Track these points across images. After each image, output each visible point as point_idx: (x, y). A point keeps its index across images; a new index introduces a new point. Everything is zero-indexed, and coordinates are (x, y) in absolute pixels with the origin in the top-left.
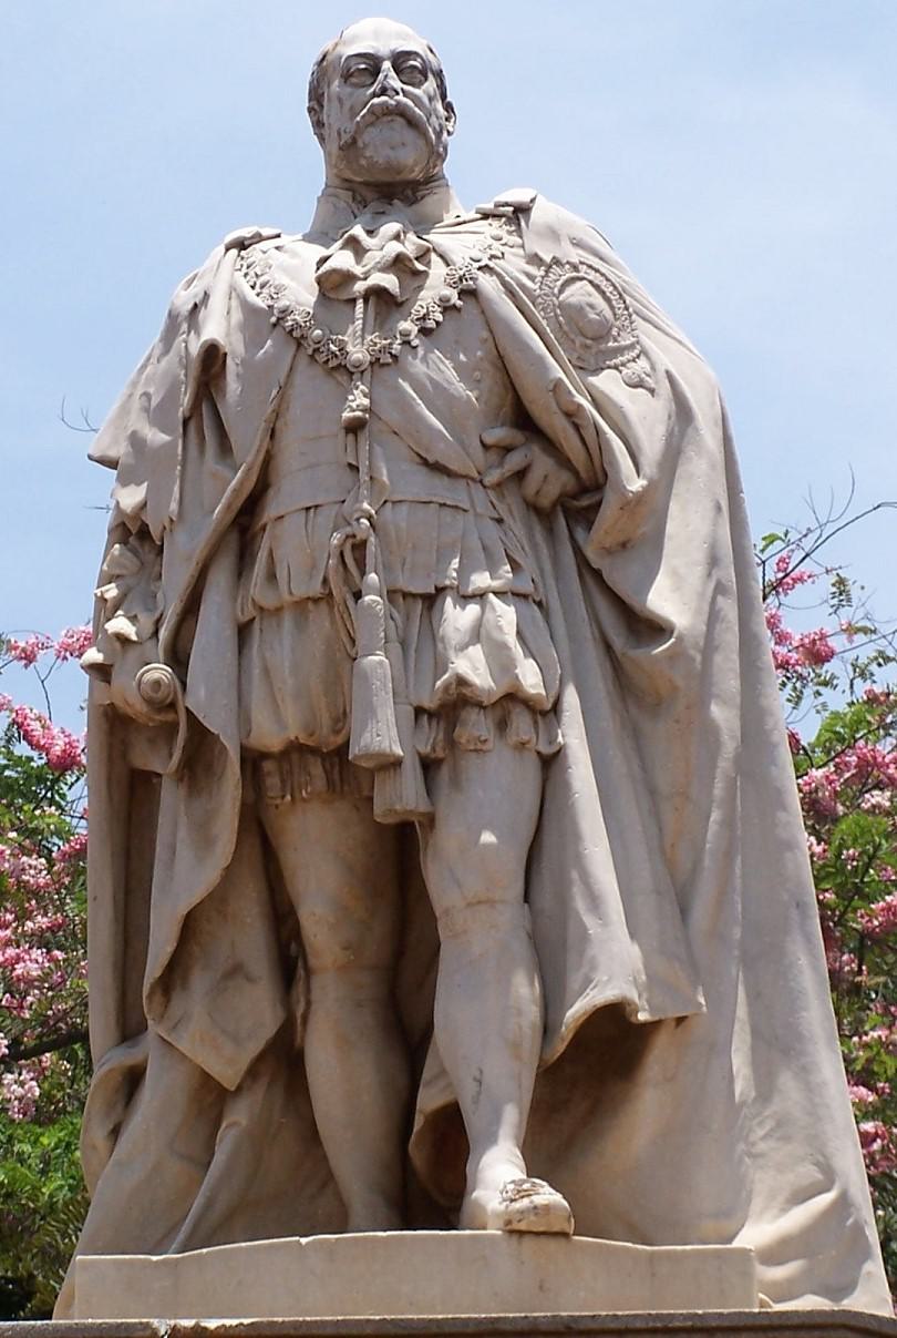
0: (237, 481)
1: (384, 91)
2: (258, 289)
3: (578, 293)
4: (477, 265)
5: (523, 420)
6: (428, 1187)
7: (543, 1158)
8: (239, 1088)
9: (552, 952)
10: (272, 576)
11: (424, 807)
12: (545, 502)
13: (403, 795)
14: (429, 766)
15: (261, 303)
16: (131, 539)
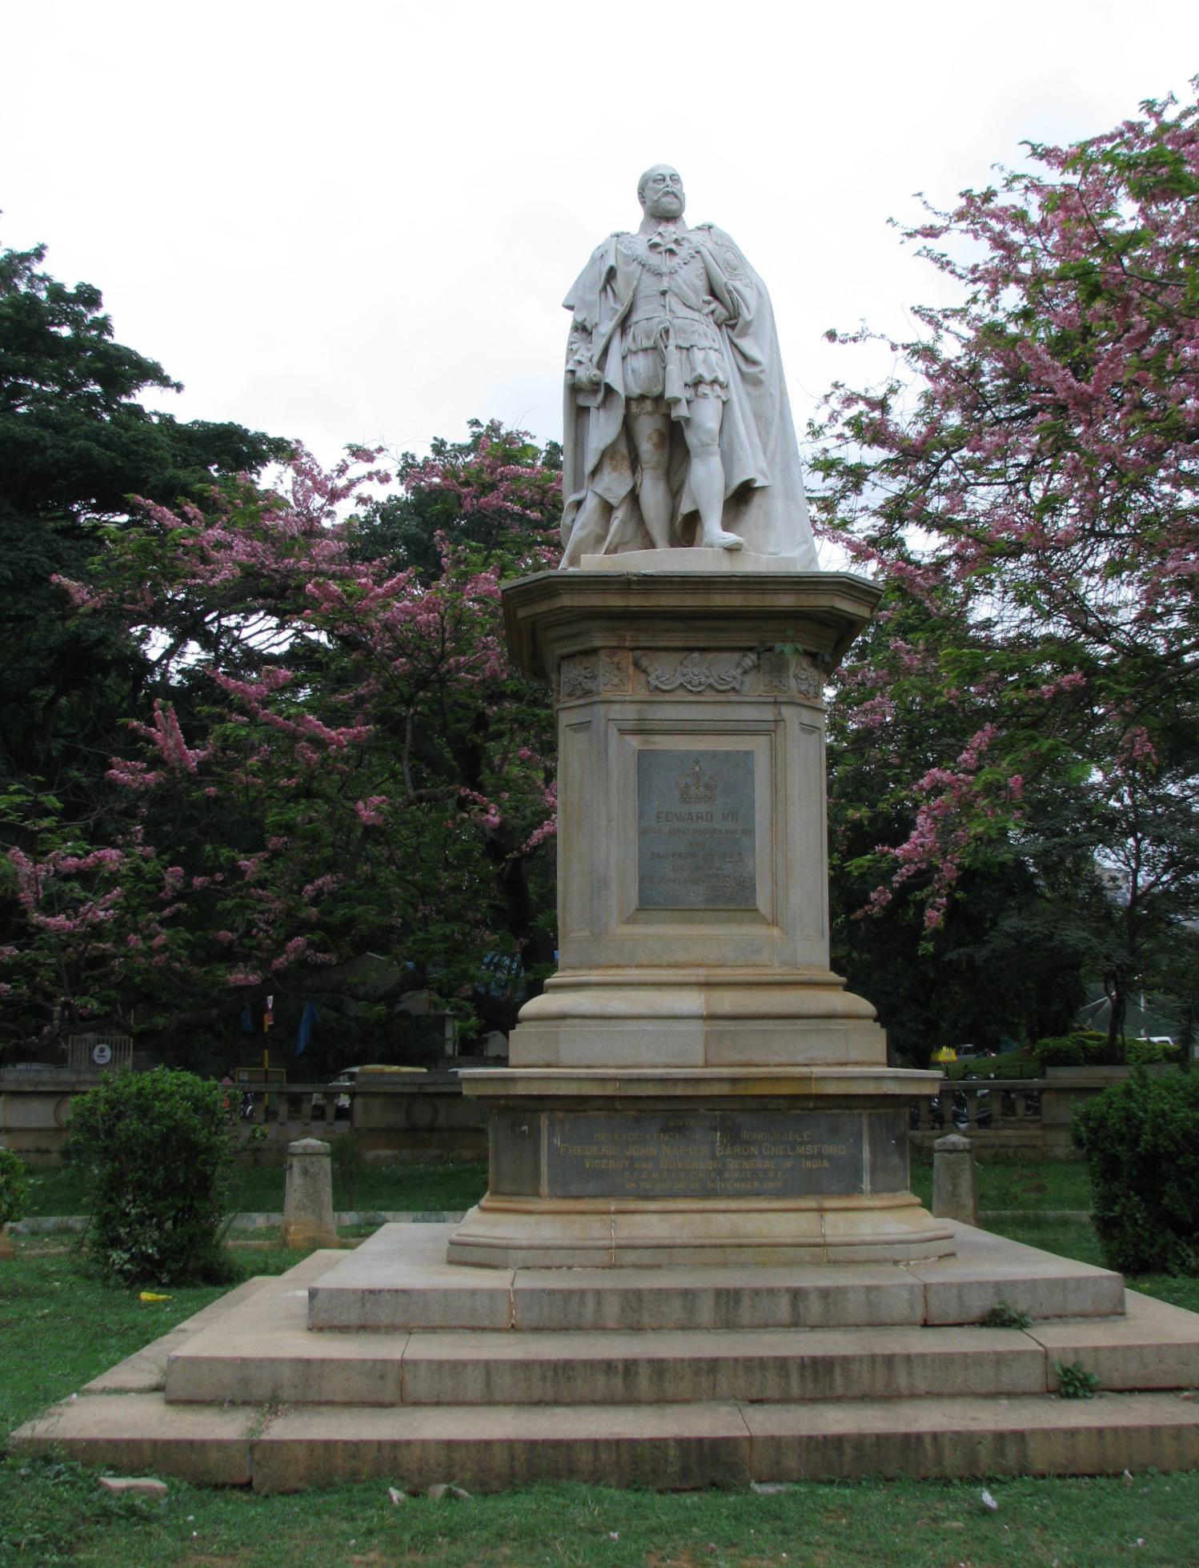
0: (621, 309)
3: (729, 256)
6: (687, 530)
9: (728, 461)
13: (682, 411)
14: (689, 402)
15: (629, 253)
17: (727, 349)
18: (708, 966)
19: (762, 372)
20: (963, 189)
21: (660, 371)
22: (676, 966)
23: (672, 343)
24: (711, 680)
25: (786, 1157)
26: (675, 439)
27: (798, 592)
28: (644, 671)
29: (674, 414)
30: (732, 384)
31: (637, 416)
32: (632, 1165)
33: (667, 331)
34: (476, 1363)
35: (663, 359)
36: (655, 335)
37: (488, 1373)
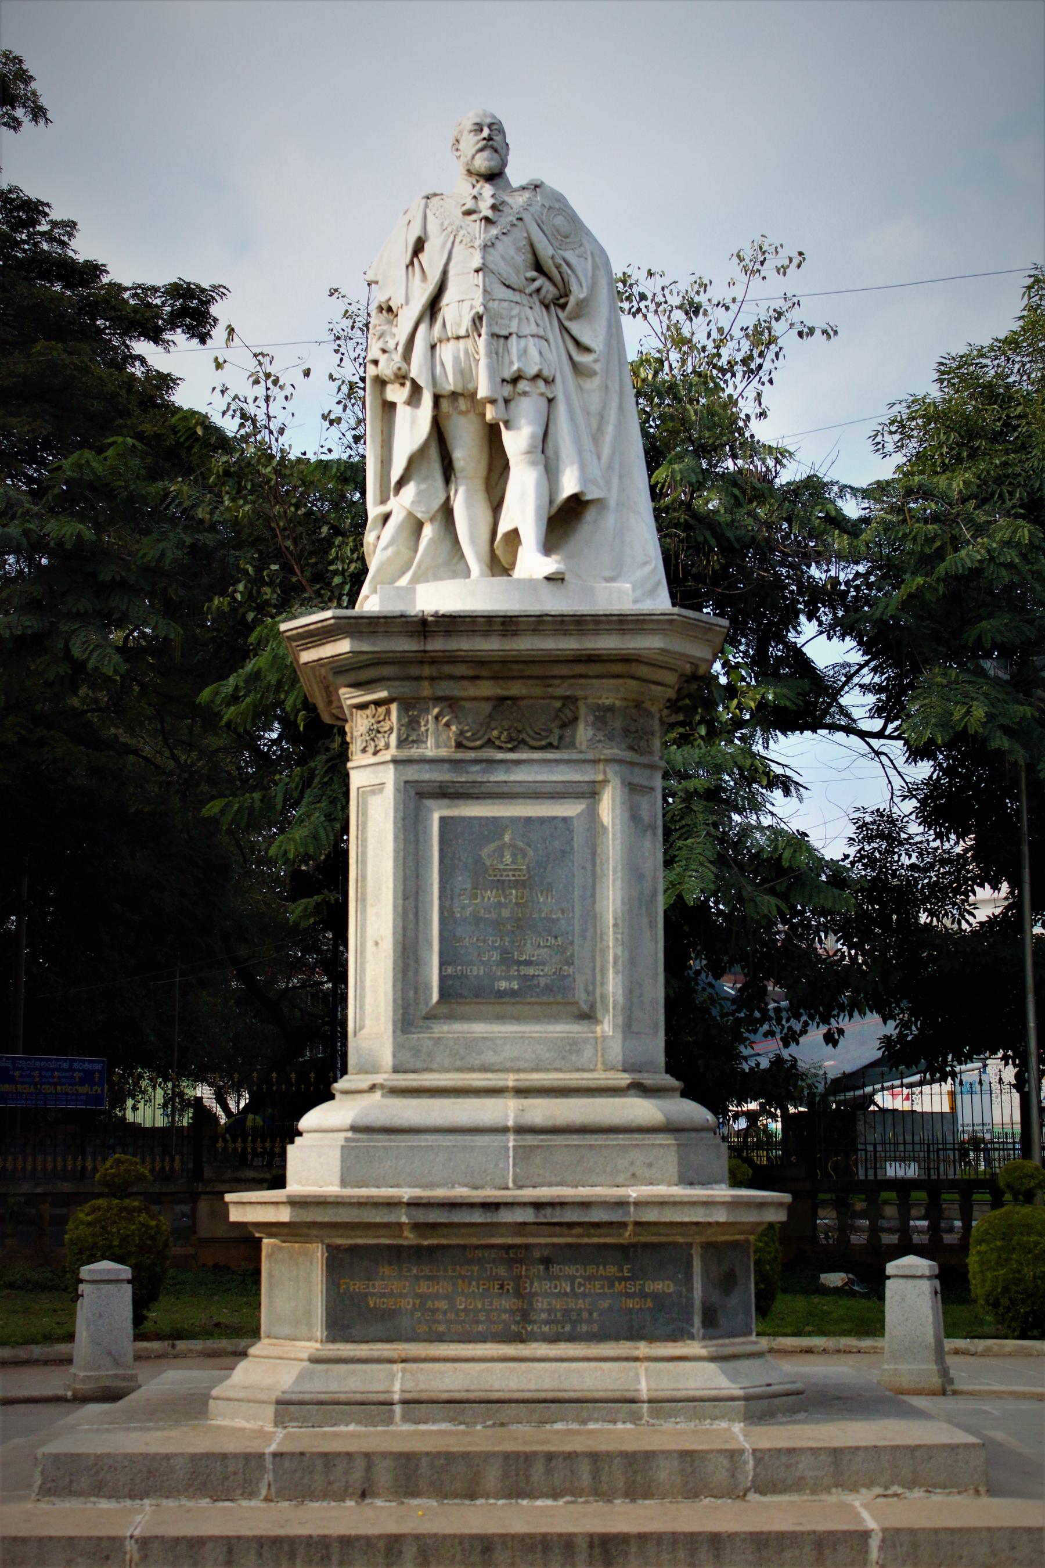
5: (538, 267)
7: (548, 547)
14: (507, 401)
17: (554, 333)
18: (519, 1071)
20: (227, 385)
22: (484, 1069)
25: (604, 1295)
27: (623, 631)
31: (448, 416)
32: (423, 1304)
34: (215, 1539)
37: (230, 1551)
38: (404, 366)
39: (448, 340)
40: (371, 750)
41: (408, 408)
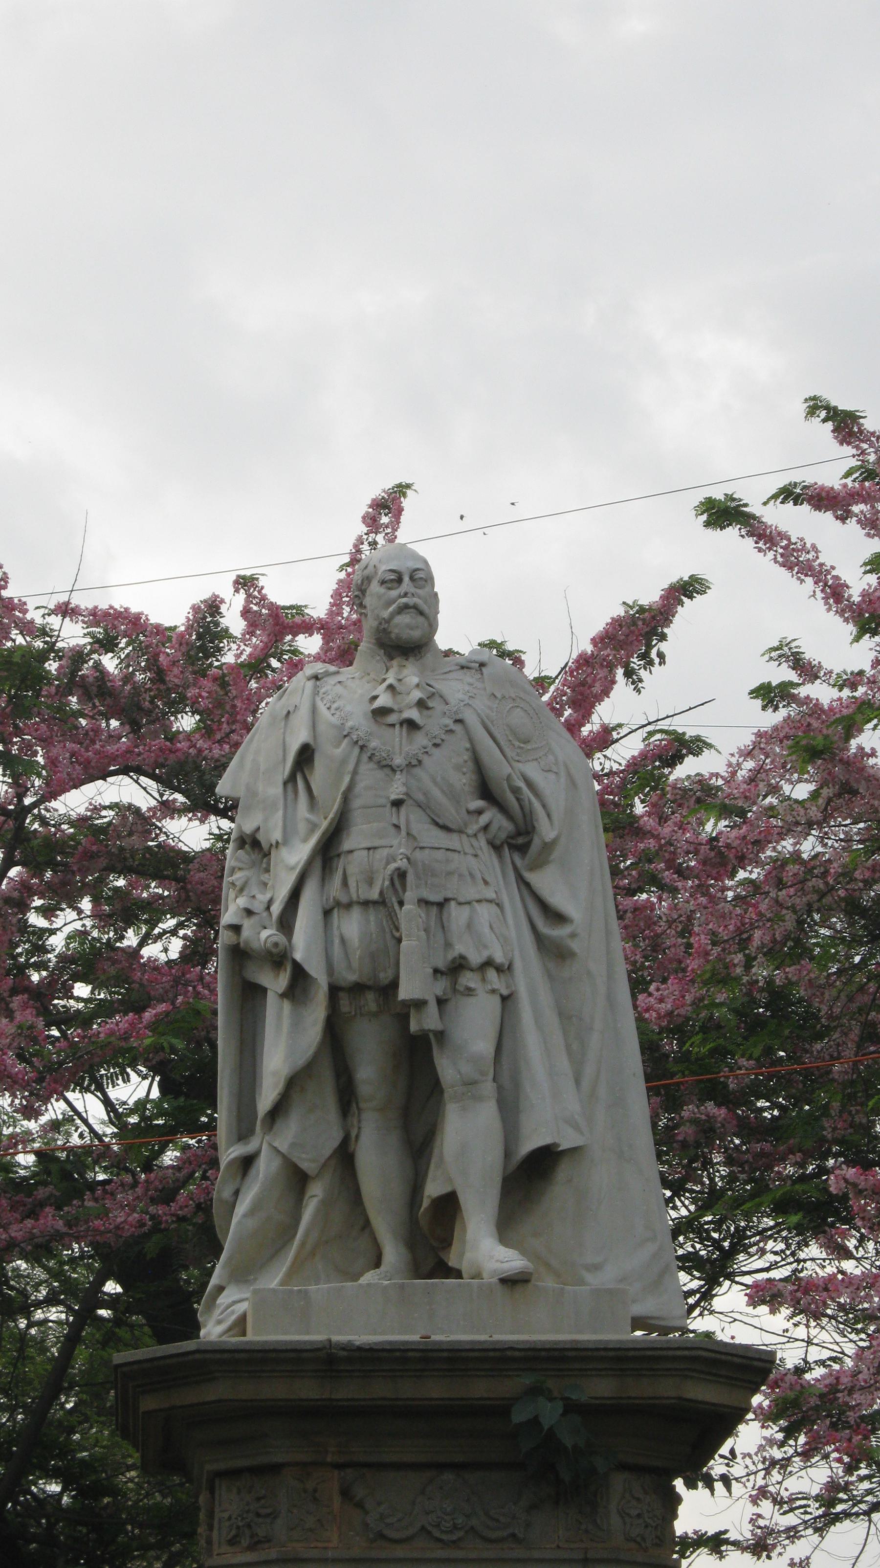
1: (406, 595)
2: (333, 711)
4: (462, 704)
5: (486, 791)
7: (506, 1226)
8: (317, 1175)
9: (510, 1108)
10: (345, 883)
11: (439, 1027)
12: (498, 842)
13: (428, 1020)
14: (441, 1002)
16: (247, 846)
17: (511, 897)
19: (573, 935)
21: (391, 943)
23: (410, 896)
24: (474, 1522)
26: (417, 1058)
28: (360, 1505)
29: (414, 1027)
30: (518, 965)
33: (402, 875)
35: (393, 918)
36: (381, 882)
38: (281, 939)
39: (349, 906)
40: (245, 1542)
41: (287, 1005)
